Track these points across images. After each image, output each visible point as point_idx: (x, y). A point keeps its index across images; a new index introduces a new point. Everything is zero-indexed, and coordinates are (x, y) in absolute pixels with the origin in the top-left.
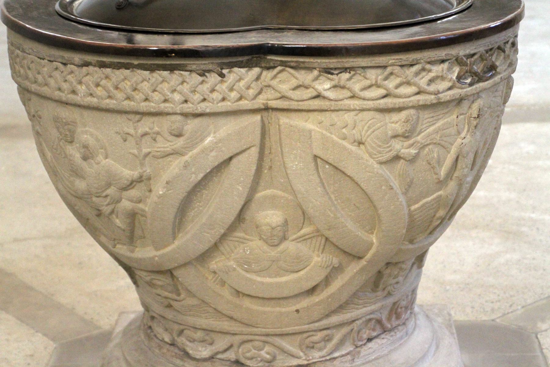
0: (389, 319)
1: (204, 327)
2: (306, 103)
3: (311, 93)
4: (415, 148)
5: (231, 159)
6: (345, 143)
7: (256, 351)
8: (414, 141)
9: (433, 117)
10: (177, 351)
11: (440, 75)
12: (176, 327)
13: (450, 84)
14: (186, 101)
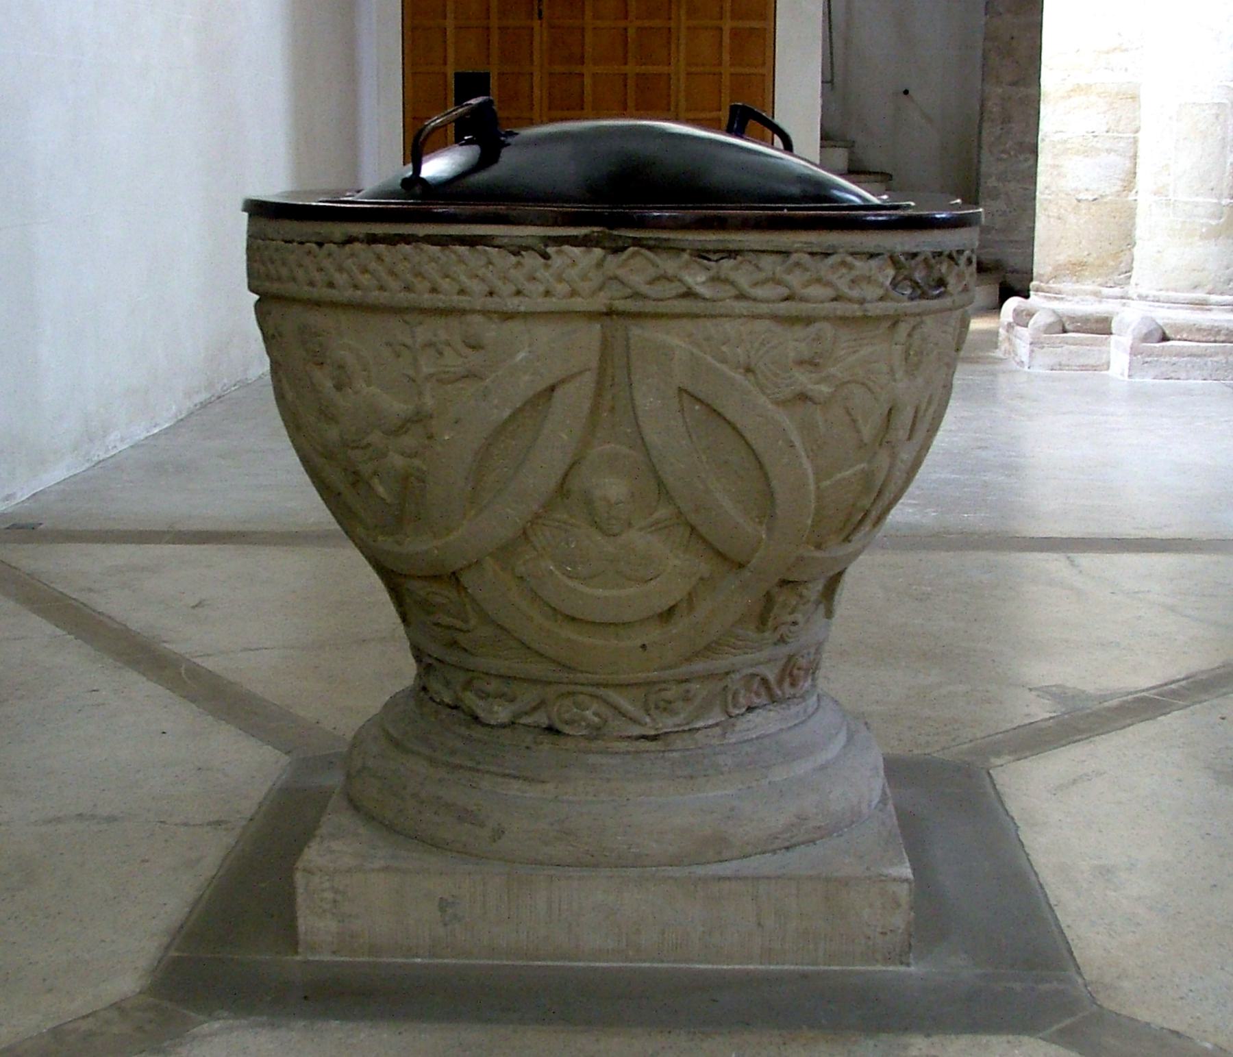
0: (780, 682)
1: (503, 671)
2: (669, 303)
3: (676, 288)
5: (552, 389)
6: (724, 368)
7: (579, 711)
10: (462, 716)
11: (868, 275)
12: (461, 677)
13: (881, 292)
14: (491, 294)
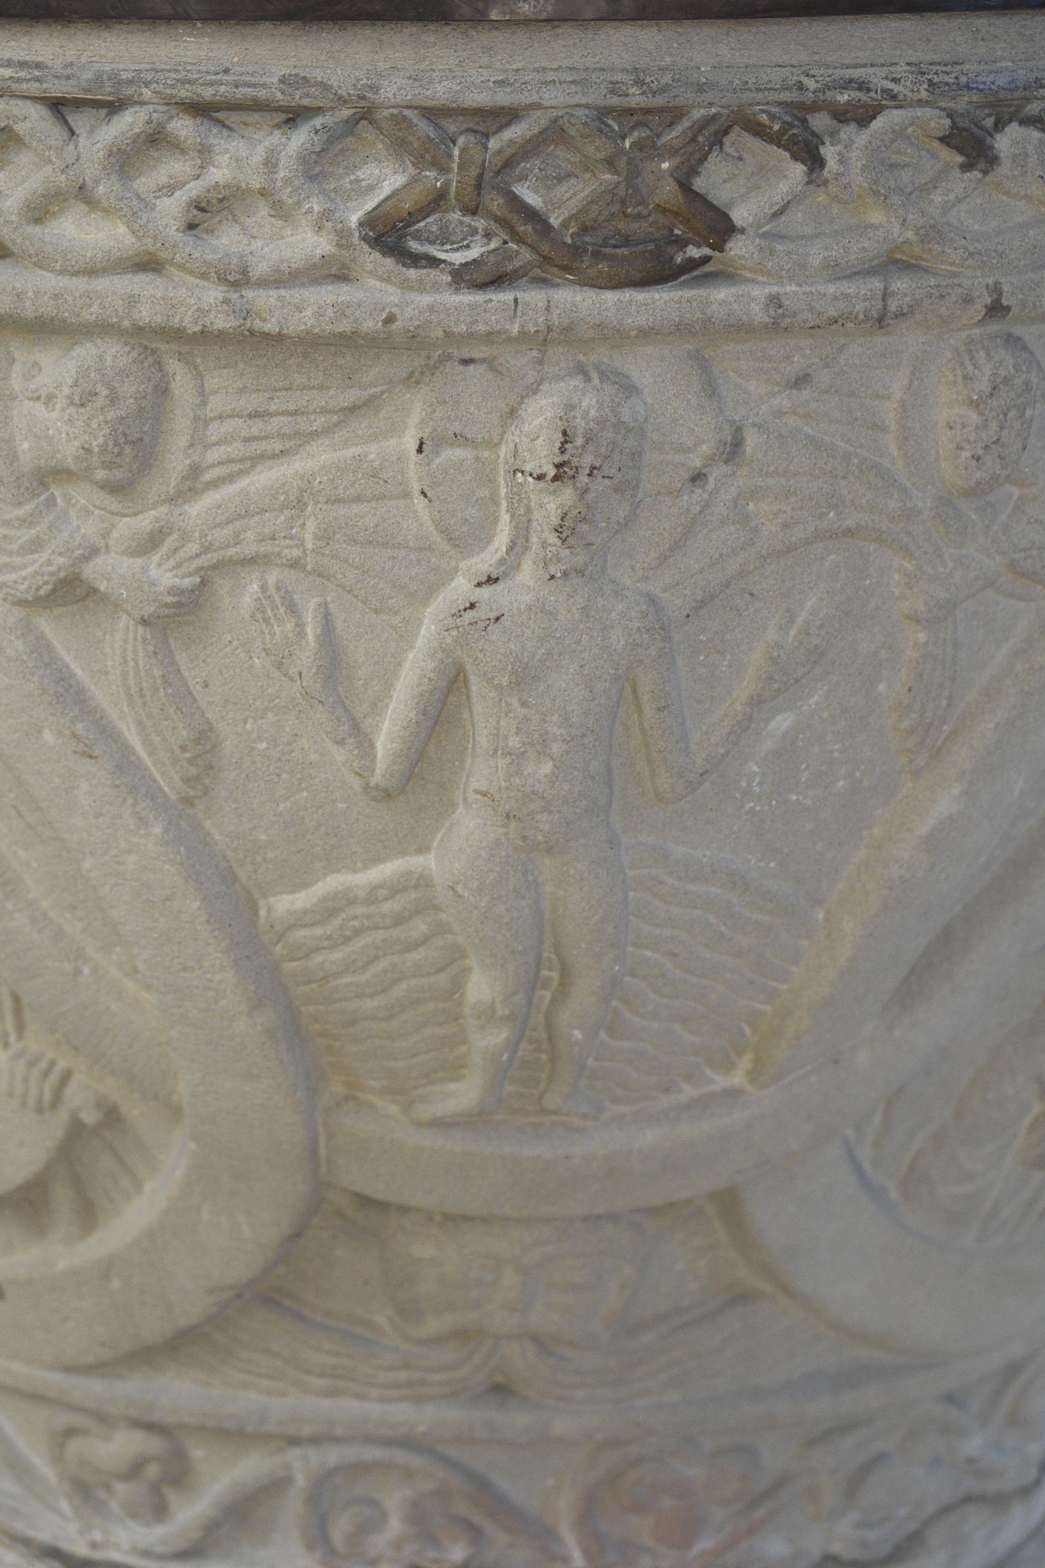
4: (172, 562)
8: (157, 520)
9: (254, 415)
13: (322, 245)
